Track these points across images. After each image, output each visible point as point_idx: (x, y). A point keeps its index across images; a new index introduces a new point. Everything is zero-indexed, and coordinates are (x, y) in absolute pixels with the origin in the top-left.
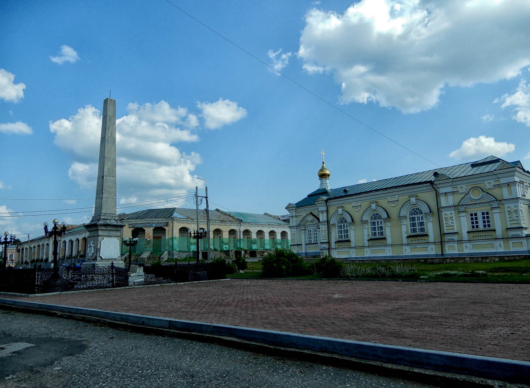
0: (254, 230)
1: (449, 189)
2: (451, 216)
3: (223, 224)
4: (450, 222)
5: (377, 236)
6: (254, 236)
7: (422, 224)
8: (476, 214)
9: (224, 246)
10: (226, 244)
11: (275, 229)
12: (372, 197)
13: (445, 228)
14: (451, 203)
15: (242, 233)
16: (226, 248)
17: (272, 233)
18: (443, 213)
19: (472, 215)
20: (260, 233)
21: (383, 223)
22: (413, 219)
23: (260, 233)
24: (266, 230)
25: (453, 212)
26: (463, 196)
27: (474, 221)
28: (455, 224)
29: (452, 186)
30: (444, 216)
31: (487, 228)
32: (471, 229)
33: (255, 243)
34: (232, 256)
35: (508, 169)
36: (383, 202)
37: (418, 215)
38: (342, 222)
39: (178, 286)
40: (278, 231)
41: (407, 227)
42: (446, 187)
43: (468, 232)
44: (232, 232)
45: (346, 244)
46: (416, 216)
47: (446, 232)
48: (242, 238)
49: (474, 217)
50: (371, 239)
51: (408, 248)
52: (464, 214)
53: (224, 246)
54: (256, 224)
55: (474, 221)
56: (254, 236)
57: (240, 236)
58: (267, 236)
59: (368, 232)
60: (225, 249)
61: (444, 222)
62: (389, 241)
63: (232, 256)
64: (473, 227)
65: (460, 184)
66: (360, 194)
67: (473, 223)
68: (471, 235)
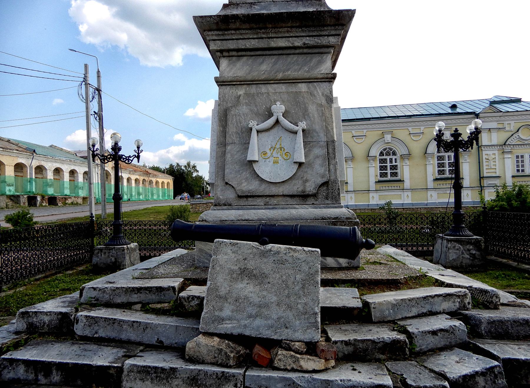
0: (50, 166)
1: (494, 125)
2: (494, 157)
3: (6, 153)
4: (492, 163)
5: (389, 178)
6: (50, 175)
7: (394, 167)
8: (522, 157)
9: (7, 188)
10: (9, 185)
11: (76, 168)
12: (386, 126)
13: (485, 171)
14: (495, 142)
15: (34, 170)
16: (10, 191)
17: (73, 173)
18: (484, 153)
19: (517, 157)
20: (57, 171)
21: (398, 161)
22: (383, 161)
23: (57, 171)
24: (66, 168)
25: (496, 152)
26: (511, 134)
27: (520, 164)
28: (497, 167)
29: (497, 121)
30: (484, 157)
31: (521, 173)
32: (516, 174)
33: (50, 186)
34: (24, 203)
35: (494, 114)
36: (402, 134)
37: (391, 157)
38: (388, 154)
39: (294, 250)
40: (81, 170)
41: (434, 167)
42: (491, 121)
43: (513, 177)
44: (19, 167)
45: (396, 184)
46: (388, 158)
47: (485, 175)
48: (34, 177)
49: (520, 159)
50: (437, 179)
51: (434, 194)
52: (510, 156)
53: (7, 188)
54: (53, 159)
55: (520, 164)
56: (50, 175)
57: (31, 174)
58: (67, 177)
59: (376, 171)
60: (8, 193)
61: (485, 164)
62: (407, 184)
63: (24, 203)
64: (518, 171)
65: (507, 120)
66: (369, 119)
67: (518, 166)
68: (516, 180)
